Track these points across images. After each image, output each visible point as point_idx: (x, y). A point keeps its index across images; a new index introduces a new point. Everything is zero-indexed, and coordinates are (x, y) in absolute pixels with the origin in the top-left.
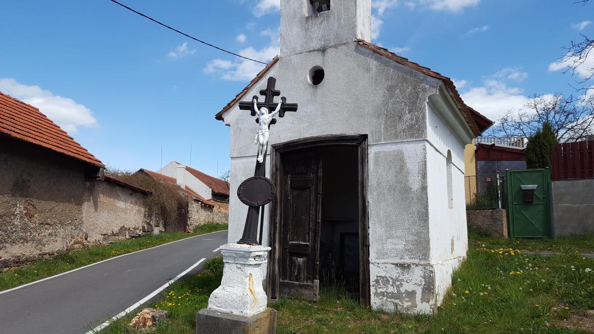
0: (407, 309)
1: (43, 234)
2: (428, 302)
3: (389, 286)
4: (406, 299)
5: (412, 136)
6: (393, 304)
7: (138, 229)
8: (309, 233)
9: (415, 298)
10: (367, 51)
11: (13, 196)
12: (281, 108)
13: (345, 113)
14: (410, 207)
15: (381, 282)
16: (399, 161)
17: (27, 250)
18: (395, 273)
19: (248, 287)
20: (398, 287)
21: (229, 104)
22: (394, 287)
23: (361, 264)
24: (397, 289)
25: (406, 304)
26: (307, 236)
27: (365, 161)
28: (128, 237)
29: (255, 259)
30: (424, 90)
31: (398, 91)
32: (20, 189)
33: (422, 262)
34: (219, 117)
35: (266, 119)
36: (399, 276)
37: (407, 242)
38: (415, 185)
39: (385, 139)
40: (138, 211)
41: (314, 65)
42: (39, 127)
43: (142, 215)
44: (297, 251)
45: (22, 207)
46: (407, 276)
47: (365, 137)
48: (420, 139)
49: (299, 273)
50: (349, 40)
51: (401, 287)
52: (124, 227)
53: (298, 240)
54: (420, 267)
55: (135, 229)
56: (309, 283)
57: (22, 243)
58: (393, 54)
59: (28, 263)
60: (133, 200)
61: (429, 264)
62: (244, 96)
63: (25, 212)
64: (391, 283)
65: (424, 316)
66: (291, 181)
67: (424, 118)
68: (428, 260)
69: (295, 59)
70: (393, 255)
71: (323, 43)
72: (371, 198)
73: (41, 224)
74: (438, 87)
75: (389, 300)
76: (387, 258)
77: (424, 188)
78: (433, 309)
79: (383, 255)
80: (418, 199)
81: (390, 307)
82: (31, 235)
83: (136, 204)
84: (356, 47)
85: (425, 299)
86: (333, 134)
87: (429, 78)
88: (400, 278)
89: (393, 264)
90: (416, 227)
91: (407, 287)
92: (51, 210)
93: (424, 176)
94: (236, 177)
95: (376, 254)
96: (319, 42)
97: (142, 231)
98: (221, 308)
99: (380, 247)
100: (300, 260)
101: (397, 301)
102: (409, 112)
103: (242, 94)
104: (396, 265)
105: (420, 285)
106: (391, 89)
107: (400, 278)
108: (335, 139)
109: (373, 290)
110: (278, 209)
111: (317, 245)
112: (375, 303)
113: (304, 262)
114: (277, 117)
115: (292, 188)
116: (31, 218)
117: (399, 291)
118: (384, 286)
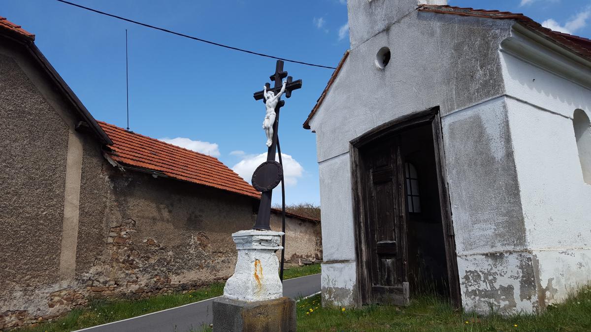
0: (505, 309)
1: (216, 261)
2: (530, 298)
3: (481, 282)
4: (502, 297)
5: (488, 94)
6: (487, 305)
7: (311, 256)
8: (394, 230)
9: (513, 295)
10: (429, 15)
11: (187, 229)
12: (286, 88)
13: (414, 89)
14: (495, 181)
15: (471, 278)
16: (477, 128)
17: (203, 275)
18: (486, 265)
19: (253, 273)
20: (491, 282)
21: (312, 111)
22: (486, 284)
23: (448, 258)
24: (490, 285)
25: (503, 304)
26: (393, 234)
27: (439, 137)
28: (300, 264)
29: (260, 243)
30: (495, 37)
31: (466, 48)
32: (193, 223)
33: (518, 248)
34: (307, 126)
35: (270, 102)
36: (491, 269)
37: (497, 225)
38: (499, 153)
39: (458, 106)
40: (309, 240)
41: (380, 48)
42: (210, 172)
43: (314, 243)
44: (386, 252)
45: (196, 238)
46: (501, 268)
47: (436, 109)
48: (498, 96)
49: (389, 276)
50: (411, 10)
51: (495, 282)
52: (295, 254)
53: (386, 239)
54: (515, 255)
55: (307, 256)
56: (400, 286)
57: (198, 269)
58: (456, 7)
59: (204, 287)
60: (303, 229)
61: (526, 249)
62: (324, 100)
63: (198, 242)
64: (482, 279)
65: (527, 317)
66: (374, 176)
67: (499, 69)
68: (524, 245)
69: (363, 48)
70: (482, 243)
71: (387, 22)
72: (450, 179)
73: (214, 252)
74: (511, 29)
75: (482, 299)
76: (476, 248)
77: (510, 155)
78: (537, 307)
79: (471, 245)
80: (504, 169)
81: (484, 309)
82: (205, 262)
83: (306, 232)
84: (418, 14)
85: (525, 296)
86: (403, 114)
87: (498, 22)
88: (492, 271)
89: (483, 254)
90: (505, 205)
91: (502, 282)
92: (222, 240)
93: (508, 139)
94: (324, 182)
95: (462, 245)
96: (383, 22)
97: (315, 259)
98: (231, 296)
99: (466, 236)
100: (389, 261)
101: (492, 300)
102: (481, 68)
103: (322, 98)
104: (486, 255)
105: (518, 278)
106: (458, 48)
107: (492, 271)
108: (407, 120)
109: (463, 289)
110: (361, 208)
111: (403, 243)
112: (467, 304)
113: (393, 263)
114: (284, 98)
115: (375, 183)
116: (204, 247)
117: (492, 287)
118: (475, 283)
